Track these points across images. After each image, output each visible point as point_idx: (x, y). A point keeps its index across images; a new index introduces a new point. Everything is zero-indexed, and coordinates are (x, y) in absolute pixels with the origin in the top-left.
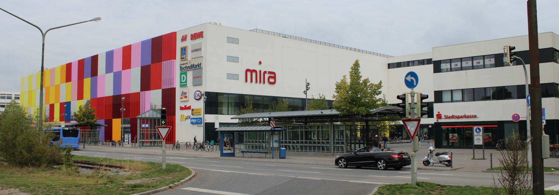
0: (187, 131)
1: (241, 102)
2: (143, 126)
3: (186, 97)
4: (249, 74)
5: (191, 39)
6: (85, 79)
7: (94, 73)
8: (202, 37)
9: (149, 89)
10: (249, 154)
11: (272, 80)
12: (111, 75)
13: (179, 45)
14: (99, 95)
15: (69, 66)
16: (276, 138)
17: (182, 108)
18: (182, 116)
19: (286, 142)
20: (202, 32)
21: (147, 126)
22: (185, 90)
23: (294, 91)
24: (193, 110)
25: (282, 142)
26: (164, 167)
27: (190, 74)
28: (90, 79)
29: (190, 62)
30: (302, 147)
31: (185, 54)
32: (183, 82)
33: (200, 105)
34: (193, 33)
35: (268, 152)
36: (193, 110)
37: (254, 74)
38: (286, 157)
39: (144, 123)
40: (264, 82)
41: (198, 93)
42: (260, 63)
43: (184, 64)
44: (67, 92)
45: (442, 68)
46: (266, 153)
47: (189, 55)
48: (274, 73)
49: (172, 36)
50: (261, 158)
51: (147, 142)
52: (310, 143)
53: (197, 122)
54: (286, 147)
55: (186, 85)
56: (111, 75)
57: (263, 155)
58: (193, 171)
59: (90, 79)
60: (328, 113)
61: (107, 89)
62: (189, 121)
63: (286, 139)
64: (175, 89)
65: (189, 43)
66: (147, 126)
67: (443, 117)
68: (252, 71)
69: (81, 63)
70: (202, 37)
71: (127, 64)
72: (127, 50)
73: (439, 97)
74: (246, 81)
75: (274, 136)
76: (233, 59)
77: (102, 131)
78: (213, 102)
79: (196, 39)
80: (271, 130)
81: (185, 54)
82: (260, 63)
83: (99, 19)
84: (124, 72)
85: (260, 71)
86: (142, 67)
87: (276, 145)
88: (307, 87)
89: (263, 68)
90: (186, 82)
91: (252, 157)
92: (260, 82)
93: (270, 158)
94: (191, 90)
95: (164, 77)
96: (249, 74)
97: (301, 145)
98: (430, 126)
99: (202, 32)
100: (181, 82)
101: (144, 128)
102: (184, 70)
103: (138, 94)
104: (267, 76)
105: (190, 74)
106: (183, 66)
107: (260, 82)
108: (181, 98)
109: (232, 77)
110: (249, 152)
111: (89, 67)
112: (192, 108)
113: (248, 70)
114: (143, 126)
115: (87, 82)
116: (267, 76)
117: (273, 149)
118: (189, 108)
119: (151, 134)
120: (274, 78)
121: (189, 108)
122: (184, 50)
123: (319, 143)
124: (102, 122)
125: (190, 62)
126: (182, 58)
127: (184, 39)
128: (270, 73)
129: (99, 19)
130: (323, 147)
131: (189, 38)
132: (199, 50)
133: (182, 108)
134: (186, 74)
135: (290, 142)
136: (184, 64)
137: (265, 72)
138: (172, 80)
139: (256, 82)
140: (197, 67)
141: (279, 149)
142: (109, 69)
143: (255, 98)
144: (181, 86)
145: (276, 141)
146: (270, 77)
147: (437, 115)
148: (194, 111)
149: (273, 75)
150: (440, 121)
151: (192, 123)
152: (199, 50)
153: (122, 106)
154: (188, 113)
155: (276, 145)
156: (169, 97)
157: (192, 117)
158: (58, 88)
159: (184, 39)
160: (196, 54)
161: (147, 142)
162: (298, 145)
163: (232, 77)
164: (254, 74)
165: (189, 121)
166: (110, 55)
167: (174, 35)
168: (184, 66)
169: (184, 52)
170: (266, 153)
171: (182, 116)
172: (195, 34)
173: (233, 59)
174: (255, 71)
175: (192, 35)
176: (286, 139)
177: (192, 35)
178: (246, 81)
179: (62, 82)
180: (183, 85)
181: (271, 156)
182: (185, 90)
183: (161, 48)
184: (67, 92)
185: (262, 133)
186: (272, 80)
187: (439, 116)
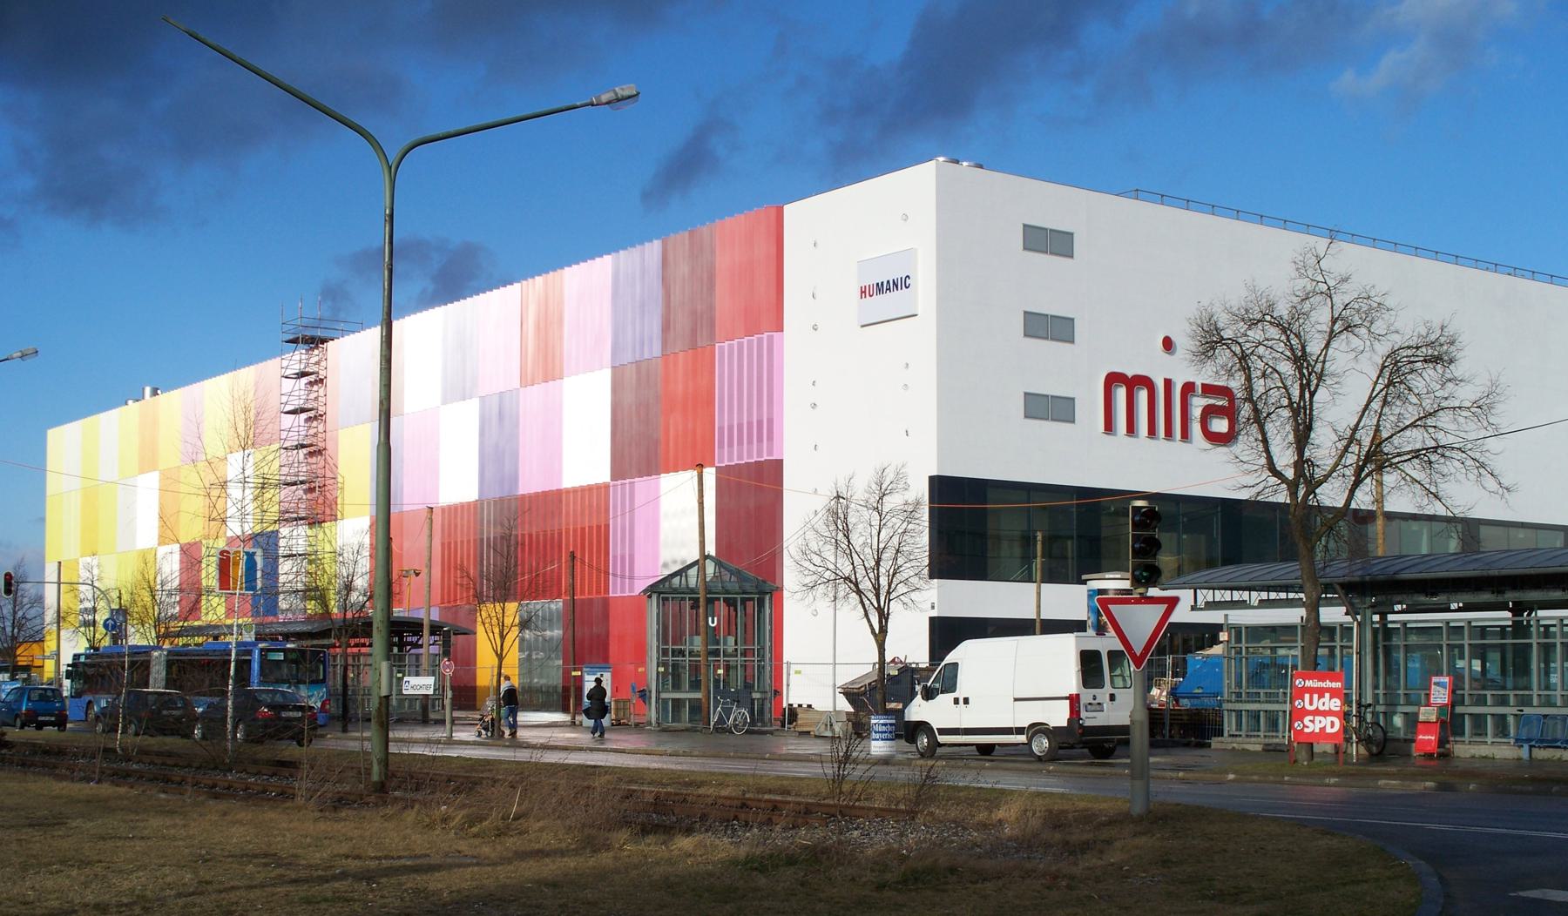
4: (1121, 393)
11: (1220, 425)
37: (1142, 396)
40: (1185, 435)
68: (1134, 383)
76: (1050, 328)
85: (1168, 383)
92: (1169, 433)
103: (595, 495)
104: (1198, 404)
109: (1048, 408)
113: (1113, 379)
116: (1198, 404)
128: (1208, 390)
137: (1188, 388)
139: (1152, 432)
146: (1208, 412)
156: (752, 503)
163: (1048, 408)
164: (1142, 396)
173: (1050, 328)
174: (1146, 382)
178: (1109, 427)
186: (1220, 425)
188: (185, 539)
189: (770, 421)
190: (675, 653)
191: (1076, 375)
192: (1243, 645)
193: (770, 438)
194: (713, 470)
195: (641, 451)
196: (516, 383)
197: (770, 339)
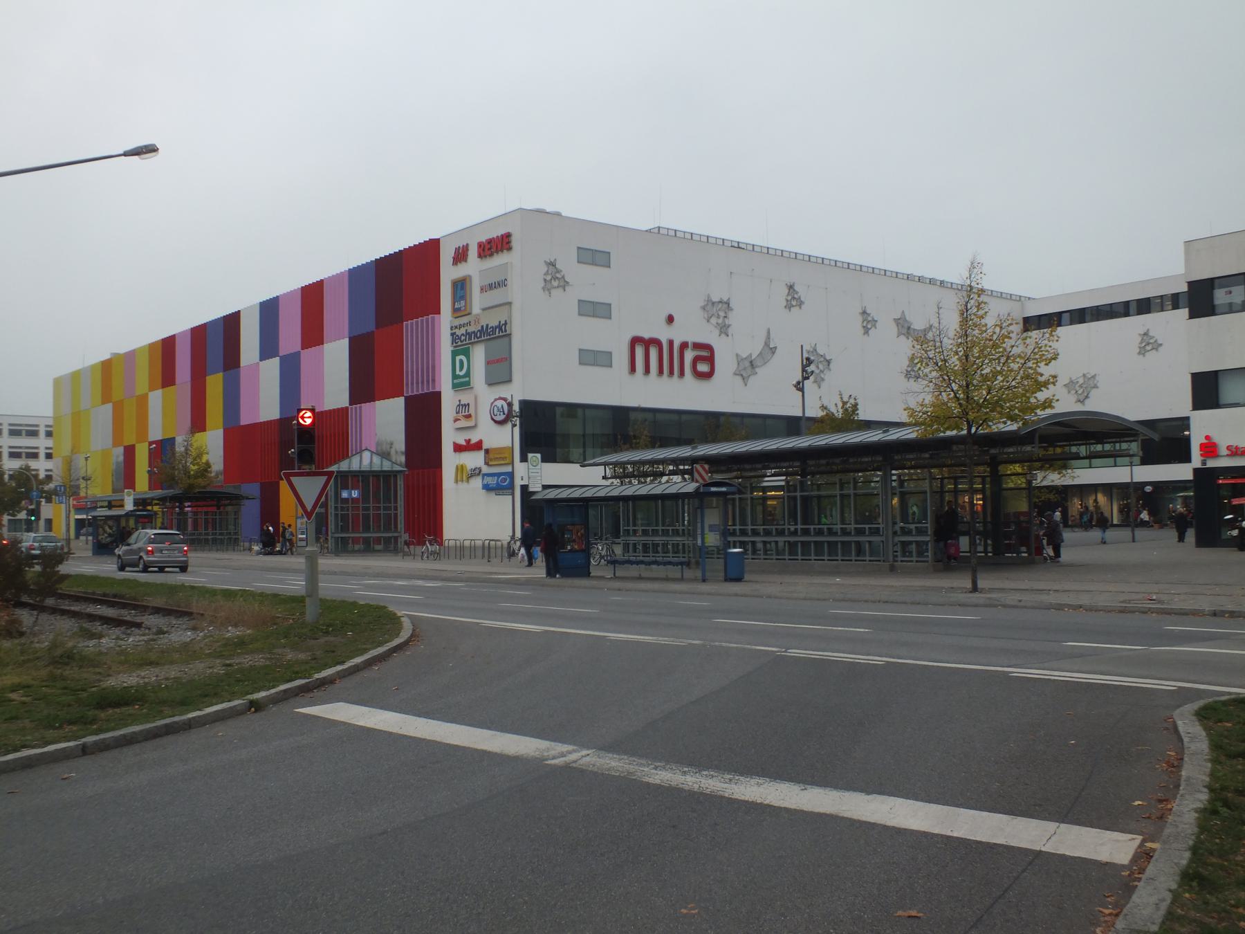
0: (476, 514)
1: (618, 428)
2: (345, 494)
3: (469, 416)
4: (639, 351)
5: (480, 256)
6: (208, 378)
7: (232, 359)
8: (510, 249)
9: (372, 398)
10: (633, 571)
11: (703, 367)
12: (274, 364)
13: (448, 273)
14: (245, 420)
15: (168, 344)
16: (712, 517)
17: (458, 448)
18: (460, 469)
19: (744, 533)
20: (508, 235)
21: (355, 494)
22: (466, 398)
23: (770, 395)
24: (487, 451)
25: (733, 534)
26: (311, 612)
27: (479, 354)
28: (221, 375)
29: (477, 321)
30: (792, 546)
31: (463, 298)
32: (460, 377)
33: (506, 437)
34: (483, 239)
35: (692, 561)
36: (487, 451)
37: (653, 353)
38: (747, 577)
39: (345, 487)
40: (682, 374)
41: (500, 403)
42: (670, 319)
43: (460, 326)
44: (162, 414)
45: (1217, 302)
46: (682, 564)
47: (477, 301)
48: (708, 348)
49: (428, 251)
50: (667, 579)
51: (356, 540)
52: (820, 532)
53: (501, 485)
54: (742, 544)
55: (468, 383)
56: (274, 364)
57: (674, 572)
58: (406, 623)
59: (221, 375)
60: (876, 439)
61: (265, 404)
62: (477, 482)
63: (743, 523)
64: (439, 394)
65: (473, 267)
66: (355, 494)
67: (1223, 451)
68: (648, 343)
69: (199, 334)
70: (510, 249)
71: (313, 335)
72: (313, 295)
73: (1207, 390)
74: (633, 369)
75: (707, 512)
76: (595, 310)
77: (250, 511)
78: (544, 428)
79: (491, 255)
80: (696, 494)
81: (463, 298)
82: (670, 319)
83: (150, 149)
84: (307, 355)
85: (671, 343)
86: (351, 339)
87: (712, 539)
88: (804, 370)
89: (678, 334)
90: (468, 374)
91: (640, 578)
92: (671, 373)
93: (695, 580)
94: (485, 397)
95: (409, 365)
96: (639, 351)
97: (792, 539)
98: (1148, 489)
99: (508, 235)
100: (455, 376)
101: (346, 500)
102: (462, 346)
103: (343, 412)
104: (689, 355)
105: (479, 354)
106: (459, 332)
107: (671, 373)
108: (456, 420)
109: (594, 358)
110: (632, 563)
111: (216, 343)
112: (485, 446)
113: (635, 341)
114: (345, 494)
115: (215, 384)
116: (689, 355)
117: (704, 552)
118: (478, 446)
119: (366, 517)
120: (710, 360)
121: (478, 446)
122: (461, 286)
123: (845, 532)
124: (252, 489)
125: (477, 321)
126: (455, 310)
127: (461, 256)
128: (697, 346)
129: (150, 149)
130: (858, 543)
131: (473, 252)
132: (502, 284)
133: (458, 448)
134: (467, 353)
135: (755, 533)
136: (460, 326)
137: (684, 346)
138: (431, 371)
139: (661, 372)
140: (497, 335)
141: (722, 551)
142: (268, 348)
143: (659, 417)
144: (455, 386)
145: (712, 528)
146: (696, 360)
147: (1202, 446)
148: (491, 456)
149: (704, 353)
150: (1211, 463)
151: (487, 488)
152: (502, 284)
153: (308, 444)
154: (474, 460)
155: (712, 539)
156: (424, 417)
157: (485, 469)
158: (142, 401)
159: (461, 256)
160: (496, 297)
161: (356, 540)
162: (781, 539)
163: (594, 358)
164: (653, 353)
165: (477, 482)
166: (269, 309)
167: (431, 248)
168: (463, 331)
169: (460, 293)
170: (682, 564)
171: (460, 469)
172: (490, 241)
173: (595, 310)
174: (656, 342)
175: (480, 245)
176: (743, 523)
177: (480, 245)
178: (633, 369)
179: (152, 388)
180: (462, 383)
181: (699, 574)
182: (466, 398)
183: (401, 286)
184: (162, 414)
185: (668, 503)
186: (703, 367)
187: (1210, 449)
188: (127, 443)
189: (434, 367)
190: (389, 509)
191: (613, 338)
192: (660, 528)
193: (434, 380)
194: (399, 402)
195: (365, 385)
196: (298, 348)
197: (433, 319)
